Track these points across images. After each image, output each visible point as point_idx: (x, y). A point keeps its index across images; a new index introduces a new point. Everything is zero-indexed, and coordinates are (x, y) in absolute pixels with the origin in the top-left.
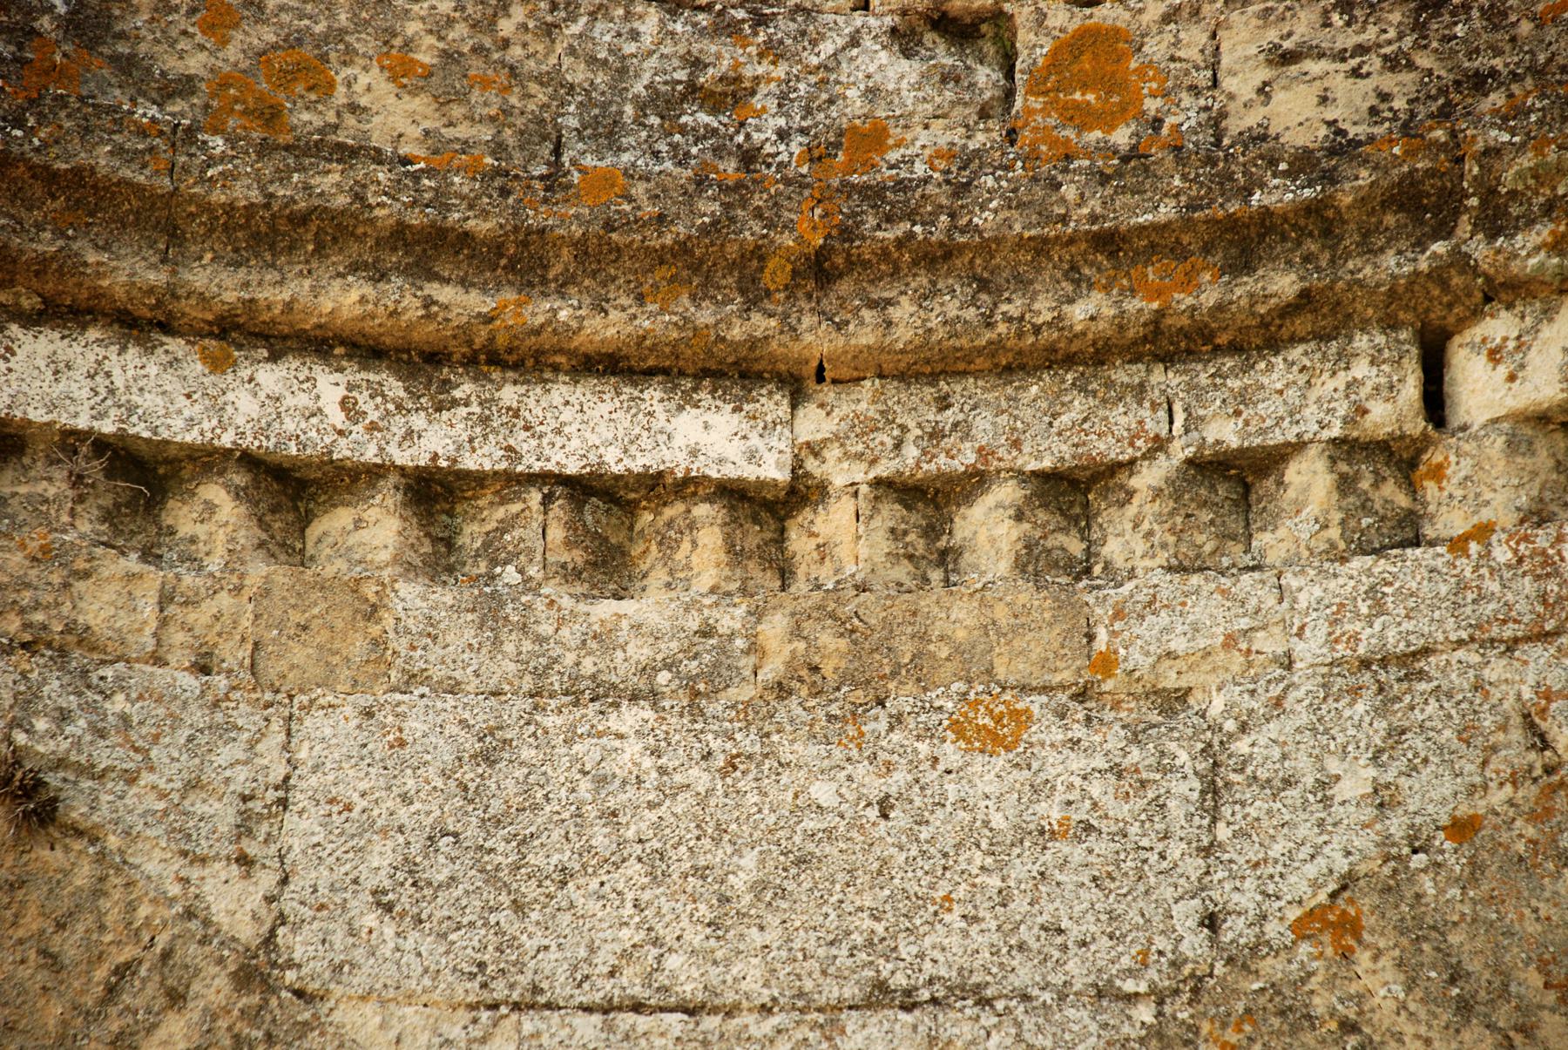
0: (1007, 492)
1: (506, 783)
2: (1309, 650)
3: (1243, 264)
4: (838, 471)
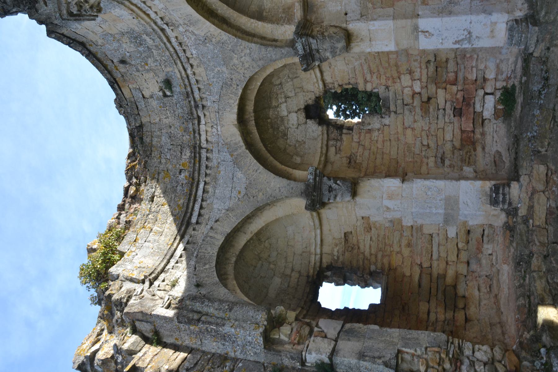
0: (207, 171)
1: (219, 198)
2: (217, 155)
3: (196, 157)
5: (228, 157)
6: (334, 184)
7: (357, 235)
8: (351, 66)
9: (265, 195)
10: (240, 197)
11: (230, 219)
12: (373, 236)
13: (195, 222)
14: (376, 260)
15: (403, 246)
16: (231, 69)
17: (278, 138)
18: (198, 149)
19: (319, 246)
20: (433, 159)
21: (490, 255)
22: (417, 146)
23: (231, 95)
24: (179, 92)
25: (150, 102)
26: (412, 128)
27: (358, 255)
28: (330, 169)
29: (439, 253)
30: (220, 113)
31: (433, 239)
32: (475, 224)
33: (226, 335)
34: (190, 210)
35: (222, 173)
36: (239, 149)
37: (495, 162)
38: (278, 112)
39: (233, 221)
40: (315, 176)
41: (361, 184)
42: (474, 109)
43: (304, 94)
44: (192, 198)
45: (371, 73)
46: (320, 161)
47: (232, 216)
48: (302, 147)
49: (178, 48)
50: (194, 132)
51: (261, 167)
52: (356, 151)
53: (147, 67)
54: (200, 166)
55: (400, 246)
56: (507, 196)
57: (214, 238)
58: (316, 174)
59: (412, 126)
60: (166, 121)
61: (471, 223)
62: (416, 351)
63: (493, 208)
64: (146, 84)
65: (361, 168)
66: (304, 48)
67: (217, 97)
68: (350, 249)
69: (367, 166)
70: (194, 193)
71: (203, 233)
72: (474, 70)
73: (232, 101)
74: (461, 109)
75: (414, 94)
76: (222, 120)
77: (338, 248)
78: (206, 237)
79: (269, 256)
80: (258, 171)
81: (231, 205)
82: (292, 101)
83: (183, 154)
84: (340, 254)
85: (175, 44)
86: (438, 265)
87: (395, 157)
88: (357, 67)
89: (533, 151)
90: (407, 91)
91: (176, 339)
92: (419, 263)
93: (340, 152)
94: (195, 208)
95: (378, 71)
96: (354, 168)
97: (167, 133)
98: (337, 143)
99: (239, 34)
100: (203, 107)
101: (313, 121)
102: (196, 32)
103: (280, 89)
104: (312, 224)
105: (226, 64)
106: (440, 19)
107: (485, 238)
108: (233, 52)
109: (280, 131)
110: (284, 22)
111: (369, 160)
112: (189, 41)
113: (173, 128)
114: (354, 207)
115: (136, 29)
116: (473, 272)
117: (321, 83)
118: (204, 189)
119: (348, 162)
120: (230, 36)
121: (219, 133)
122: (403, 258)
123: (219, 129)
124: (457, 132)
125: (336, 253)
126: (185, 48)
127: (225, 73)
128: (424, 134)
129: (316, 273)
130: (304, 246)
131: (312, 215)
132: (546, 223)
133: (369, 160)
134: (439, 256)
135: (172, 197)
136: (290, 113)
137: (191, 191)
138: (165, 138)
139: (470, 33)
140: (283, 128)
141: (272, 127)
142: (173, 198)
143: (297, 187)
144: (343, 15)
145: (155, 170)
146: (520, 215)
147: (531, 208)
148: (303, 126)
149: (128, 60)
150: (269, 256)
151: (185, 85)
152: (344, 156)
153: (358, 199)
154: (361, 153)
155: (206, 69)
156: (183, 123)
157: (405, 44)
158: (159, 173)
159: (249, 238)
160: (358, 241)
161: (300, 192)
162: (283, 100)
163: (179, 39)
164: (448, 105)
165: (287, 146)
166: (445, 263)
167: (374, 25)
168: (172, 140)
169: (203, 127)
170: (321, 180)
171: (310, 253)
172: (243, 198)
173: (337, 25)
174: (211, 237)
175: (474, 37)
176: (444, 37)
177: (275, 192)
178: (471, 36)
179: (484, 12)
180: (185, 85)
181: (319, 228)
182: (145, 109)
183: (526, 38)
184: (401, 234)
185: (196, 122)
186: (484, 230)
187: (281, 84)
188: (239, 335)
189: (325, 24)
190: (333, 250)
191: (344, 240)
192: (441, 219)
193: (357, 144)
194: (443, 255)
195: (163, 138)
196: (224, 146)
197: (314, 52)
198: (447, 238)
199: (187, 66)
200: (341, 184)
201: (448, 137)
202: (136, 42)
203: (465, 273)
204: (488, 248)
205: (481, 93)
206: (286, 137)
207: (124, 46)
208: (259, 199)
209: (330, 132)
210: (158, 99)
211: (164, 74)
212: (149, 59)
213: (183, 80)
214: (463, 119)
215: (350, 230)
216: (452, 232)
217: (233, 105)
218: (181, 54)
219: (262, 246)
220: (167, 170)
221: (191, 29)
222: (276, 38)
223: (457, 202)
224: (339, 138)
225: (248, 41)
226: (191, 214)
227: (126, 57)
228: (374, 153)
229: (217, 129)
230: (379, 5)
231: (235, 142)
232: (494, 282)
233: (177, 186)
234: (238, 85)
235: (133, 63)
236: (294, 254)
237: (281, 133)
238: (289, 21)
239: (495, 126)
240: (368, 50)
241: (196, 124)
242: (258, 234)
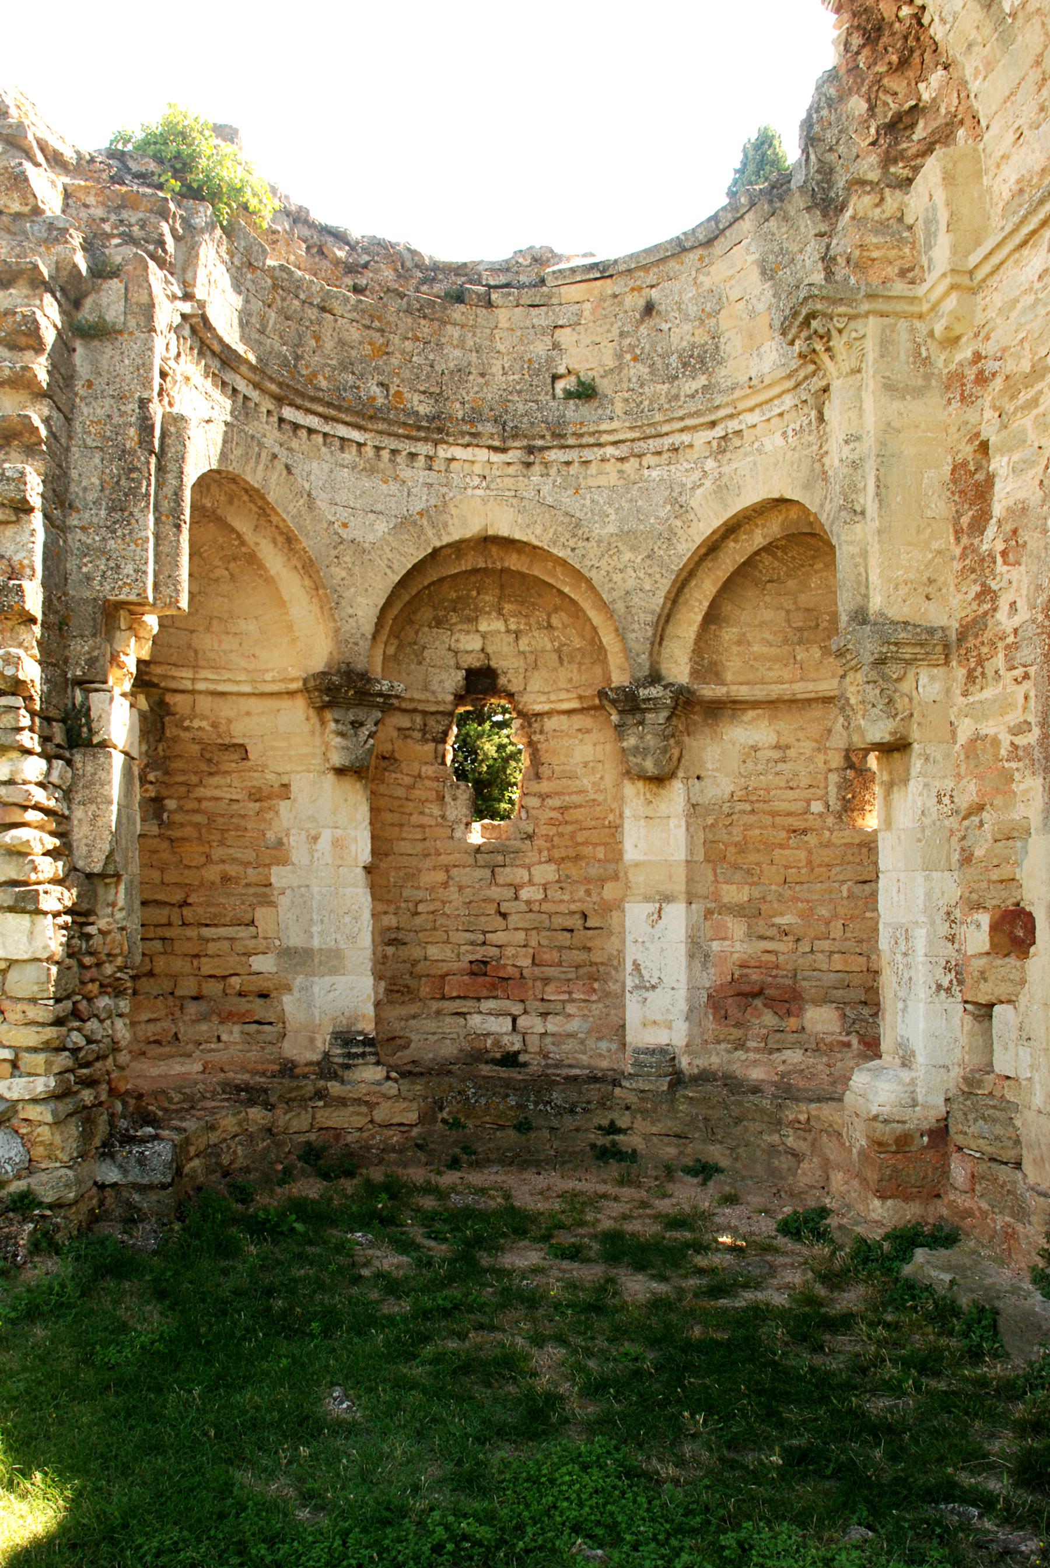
4: (369, 443)
5: (420, 506)
8: (580, 771)
12: (241, 804)
14: (188, 811)
15: (221, 867)
16: (609, 544)
17: (435, 609)
18: (435, 436)
19: (212, 687)
20: (394, 923)
21: (219, 1037)
22: (416, 892)
23: (552, 530)
24: (564, 416)
25: (545, 338)
26: (447, 882)
27: (195, 773)
29: (213, 940)
30: (514, 501)
31: (243, 927)
32: (286, 1008)
33: (126, 514)
34: (308, 405)
35: (385, 486)
37: (393, 1038)
38: (489, 613)
41: (358, 785)
42: (487, 998)
43: (522, 670)
44: (333, 412)
45: (563, 809)
49: (667, 441)
50: (474, 435)
51: (397, 579)
53: (628, 357)
54: (398, 436)
55: (223, 861)
56: (361, 1061)
57: (257, 463)
58: (390, 696)
59: (451, 883)
60: (496, 369)
61: (286, 999)
62: (121, 909)
63: (328, 1037)
64: (588, 341)
66: (649, 699)
67: (550, 500)
68: (208, 756)
70: (343, 416)
72: (565, 997)
73: (538, 532)
74: (485, 974)
75: (517, 888)
77: (208, 728)
80: (388, 571)
82: (509, 644)
83: (422, 397)
85: (677, 439)
86: (189, 939)
87: (396, 850)
88: (578, 782)
89: (441, 1098)
90: (522, 875)
91: (90, 384)
92: (190, 901)
95: (567, 823)
97: (469, 364)
99: (684, 574)
100: (528, 465)
101: (462, 683)
102: (699, 492)
103: (538, 622)
105: (622, 534)
106: (683, 939)
107: (255, 1027)
108: (648, 557)
110: (696, 663)
112: (682, 471)
113: (481, 380)
115: (723, 372)
116: (182, 1008)
117: (546, 707)
118: (349, 440)
120: (685, 559)
121: (469, 491)
122: (197, 868)
123: (478, 492)
124: (445, 968)
126: (665, 456)
127: (602, 528)
128: (437, 905)
129: (155, 680)
131: (293, 680)
132: (321, 1129)
134: (208, 941)
136: (484, 636)
137: (347, 410)
138: (457, 358)
139: (654, 987)
140: (454, 621)
141: (459, 598)
144: (697, 773)
145: (388, 323)
146: (329, 1084)
147: (342, 1102)
148: (452, 662)
149: (652, 322)
151: (582, 435)
153: (331, 777)
155: (613, 489)
156: (492, 410)
157: (637, 878)
158: (382, 331)
159: (246, 538)
160: (226, 772)
162: (513, 627)
163: (687, 450)
164: (494, 951)
166: (195, 952)
167: (677, 826)
168: (452, 373)
169: (482, 454)
170: (377, 706)
171: (196, 667)
173: (683, 761)
174: (259, 455)
175: (646, 995)
176: (647, 945)
178: (647, 989)
179: (691, 1010)
180: (582, 435)
182: (528, 323)
183: (649, 1075)
184: (249, 863)
185: (496, 443)
186: (270, 1023)
187: (550, 626)
188: (133, 547)
189: (686, 739)
190: (204, 717)
192: (295, 940)
193: (416, 773)
194: (212, 949)
195: (458, 353)
197: (638, 716)
198: (248, 955)
199: (623, 450)
200: (367, 746)
201: (433, 951)
202: (691, 356)
203: (179, 992)
204: (232, 1034)
205: (517, 1009)
207: (687, 327)
209: (439, 717)
210: (550, 360)
211: (609, 392)
212: (647, 370)
213: (594, 433)
214: (466, 977)
216: (263, 964)
217: (529, 532)
218: (653, 444)
219: (217, 562)
220: (387, 353)
221: (708, 483)
222: (664, 643)
223: (334, 971)
224: (428, 736)
225: (669, 592)
226: (298, 408)
227: (657, 320)
229: (477, 487)
230: (710, 836)
232: (168, 1049)
233: (353, 373)
234: (573, 550)
235: (643, 330)
236: (192, 632)
238: (695, 673)
239: (455, 1036)
240: (627, 813)
241: (490, 442)
242: (252, 559)
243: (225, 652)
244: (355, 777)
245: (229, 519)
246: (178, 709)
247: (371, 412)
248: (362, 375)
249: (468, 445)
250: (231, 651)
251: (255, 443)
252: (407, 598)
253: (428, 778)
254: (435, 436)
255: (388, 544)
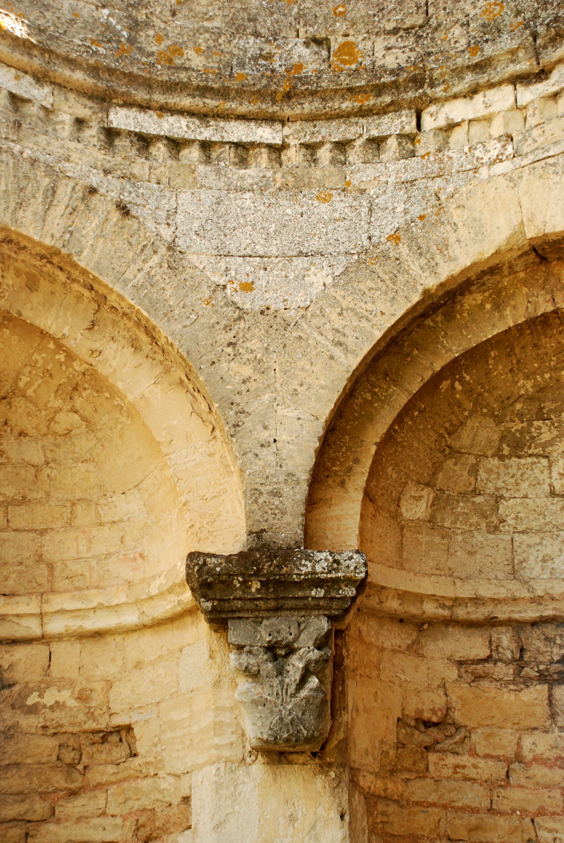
0: (328, 146)
1: (222, 209)
2: (392, 180)
4: (292, 142)
6: (301, 665)
7: (124, 780)
9: (244, 388)
10: (228, 291)
11: (134, 261)
13: (115, 125)
17: (499, 421)
19: (74, 624)
27: (43, 795)
28: (388, 644)
34: (159, 98)
35: (324, 207)
36: (423, 261)
39: (129, 275)
40: (326, 581)
41: (320, 782)
44: (211, 103)
46: (420, 598)
47: (146, 267)
48: (475, 519)
50: (479, 67)
51: (354, 362)
52: (481, 750)
57: (49, 206)
58: (336, 581)
65: (406, 775)
68: (69, 756)
69: (417, 803)
71: (68, 160)
76: (539, 172)
77: (72, 703)
78: (50, 170)
79: (22, 434)
80: (337, 352)
81: (193, 258)
83: (392, 40)
84: (50, 715)
93: (468, 678)
94: (171, 119)
96: (401, 745)
98: (507, 663)
104: (154, 591)
109: (530, 424)
111: (444, 807)
114: (219, 759)
118: (253, 145)
119: (426, 715)
121: (484, 172)
123: (499, 168)
125: (49, 698)
130: (75, 568)
133: (444, 807)
135: (210, 19)
137: (240, 93)
140: (546, 436)
142: (207, 24)
143: (283, 513)
150: (22, 434)
152: (454, 697)
154: (472, 773)
159: (70, 343)
160: (99, 786)
161: (265, 526)
165: (472, 460)
172: (227, 304)
177: (260, 427)
181: (146, 620)
191: (102, 726)
193: (510, 752)
196: (433, 200)
200: (304, 693)
206: (506, 450)
208: (224, 365)
215: (140, 748)
226: (144, 107)
228: (477, 828)
229: (498, 160)
231: (452, 240)
233: (257, 35)
236: (43, 532)
237: (521, 431)
243: (98, 559)
244: (313, 765)
245: (28, 315)
246: (18, 675)
247: (284, 87)
248: (275, 35)
249: (474, 91)
250: (108, 555)
251: (40, 173)
252: (403, 400)
253: (537, 760)
254: (411, 95)
255: (334, 303)
